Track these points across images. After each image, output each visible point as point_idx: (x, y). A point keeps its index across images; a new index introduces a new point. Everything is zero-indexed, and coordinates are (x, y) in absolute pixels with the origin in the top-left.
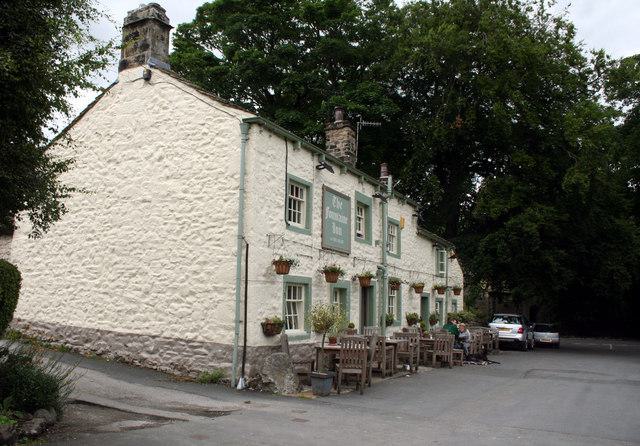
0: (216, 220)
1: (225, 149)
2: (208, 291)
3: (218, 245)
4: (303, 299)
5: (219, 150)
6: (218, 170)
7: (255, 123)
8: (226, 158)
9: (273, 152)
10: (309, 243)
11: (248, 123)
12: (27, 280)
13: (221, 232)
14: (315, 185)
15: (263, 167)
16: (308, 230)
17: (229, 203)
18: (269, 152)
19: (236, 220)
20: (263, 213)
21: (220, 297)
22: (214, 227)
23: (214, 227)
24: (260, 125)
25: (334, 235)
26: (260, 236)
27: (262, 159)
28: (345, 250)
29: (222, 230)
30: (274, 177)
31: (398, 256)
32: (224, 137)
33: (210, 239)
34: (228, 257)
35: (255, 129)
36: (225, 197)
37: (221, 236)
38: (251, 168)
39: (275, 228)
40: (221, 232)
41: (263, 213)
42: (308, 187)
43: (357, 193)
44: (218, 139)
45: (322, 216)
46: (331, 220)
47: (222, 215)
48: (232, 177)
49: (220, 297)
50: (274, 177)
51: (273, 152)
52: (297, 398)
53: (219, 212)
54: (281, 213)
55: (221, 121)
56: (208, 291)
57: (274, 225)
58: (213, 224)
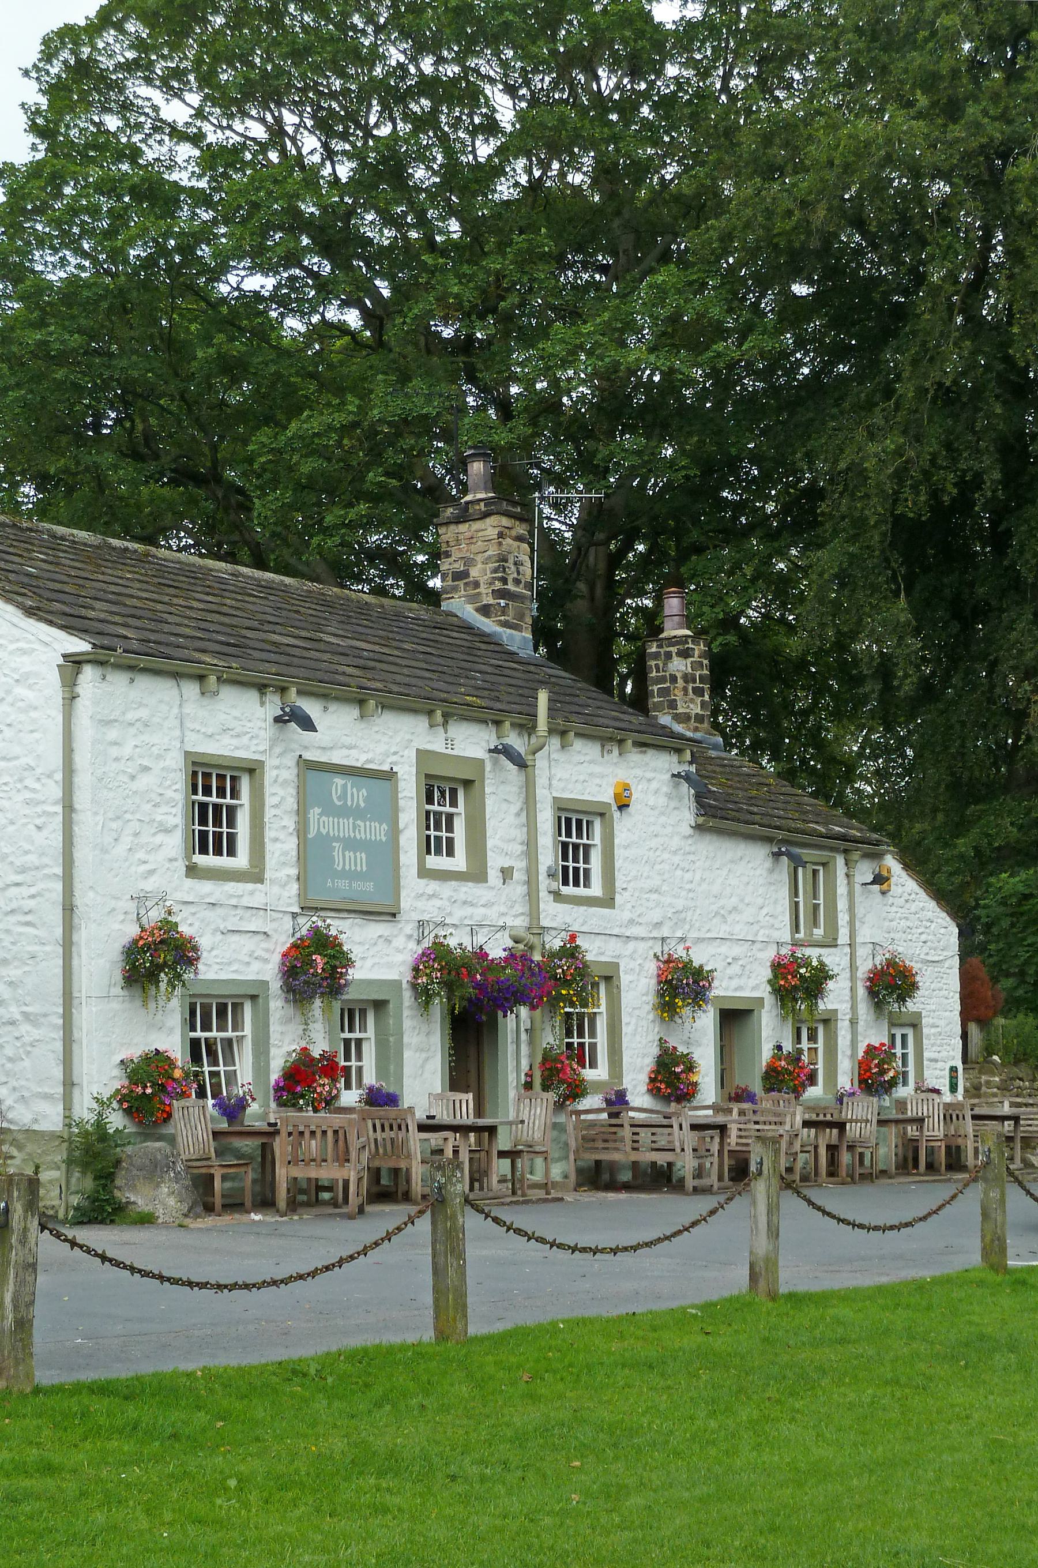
0: (23, 870)
1: (33, 714)
2: (13, 1023)
3: (28, 924)
4: (248, 1030)
5: (22, 717)
6: (23, 761)
7: (89, 662)
8: (36, 735)
9: (143, 713)
10: (257, 901)
11: (74, 663)
12: (919, 994)
13: (33, 897)
14: (270, 762)
15: (114, 752)
16: (255, 875)
17: (45, 833)
18: (130, 716)
19: (59, 871)
20: (121, 849)
21: (36, 1033)
22: (17, 884)
23: (17, 884)
24: (102, 663)
25: (344, 874)
26: (113, 903)
27: (113, 734)
28: (383, 902)
29: (33, 891)
30: (146, 769)
31: (608, 901)
32: (30, 687)
33: (12, 911)
34: (48, 948)
35: (89, 673)
36: (39, 822)
37: (31, 903)
38: (82, 759)
39: (152, 879)
40: (33, 897)
41: (121, 849)
42: (253, 770)
43: (423, 755)
44: (20, 691)
45: (301, 830)
46: (325, 841)
47: (32, 859)
48: (49, 776)
49: (36, 1033)
50: (146, 769)
51: (143, 713)
52: (208, 1230)
53: (27, 852)
54: (174, 843)
55: (24, 652)
56: (13, 1023)
57: (151, 872)
58: (19, 878)
